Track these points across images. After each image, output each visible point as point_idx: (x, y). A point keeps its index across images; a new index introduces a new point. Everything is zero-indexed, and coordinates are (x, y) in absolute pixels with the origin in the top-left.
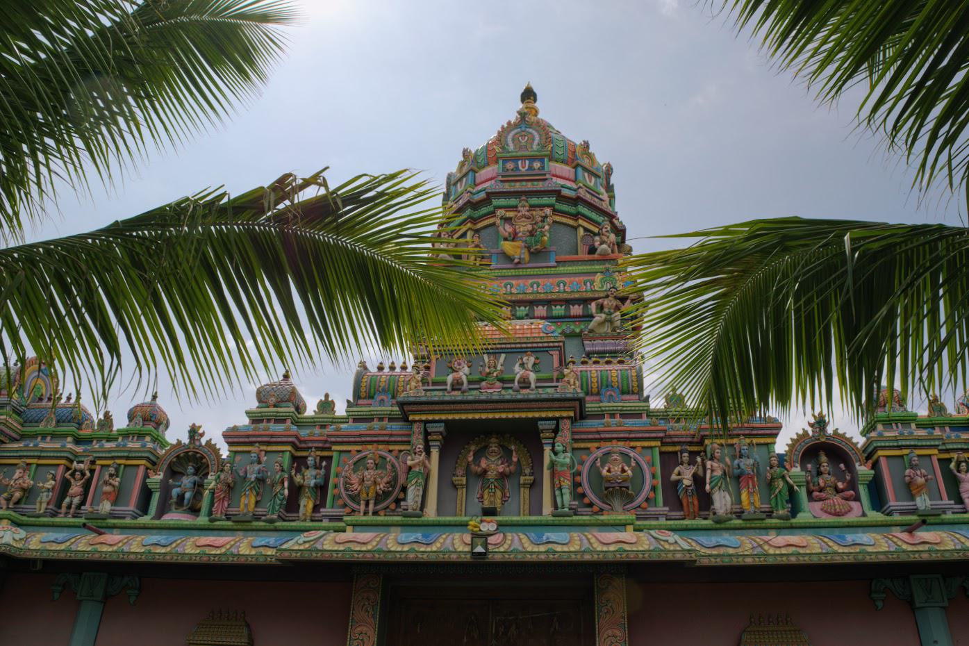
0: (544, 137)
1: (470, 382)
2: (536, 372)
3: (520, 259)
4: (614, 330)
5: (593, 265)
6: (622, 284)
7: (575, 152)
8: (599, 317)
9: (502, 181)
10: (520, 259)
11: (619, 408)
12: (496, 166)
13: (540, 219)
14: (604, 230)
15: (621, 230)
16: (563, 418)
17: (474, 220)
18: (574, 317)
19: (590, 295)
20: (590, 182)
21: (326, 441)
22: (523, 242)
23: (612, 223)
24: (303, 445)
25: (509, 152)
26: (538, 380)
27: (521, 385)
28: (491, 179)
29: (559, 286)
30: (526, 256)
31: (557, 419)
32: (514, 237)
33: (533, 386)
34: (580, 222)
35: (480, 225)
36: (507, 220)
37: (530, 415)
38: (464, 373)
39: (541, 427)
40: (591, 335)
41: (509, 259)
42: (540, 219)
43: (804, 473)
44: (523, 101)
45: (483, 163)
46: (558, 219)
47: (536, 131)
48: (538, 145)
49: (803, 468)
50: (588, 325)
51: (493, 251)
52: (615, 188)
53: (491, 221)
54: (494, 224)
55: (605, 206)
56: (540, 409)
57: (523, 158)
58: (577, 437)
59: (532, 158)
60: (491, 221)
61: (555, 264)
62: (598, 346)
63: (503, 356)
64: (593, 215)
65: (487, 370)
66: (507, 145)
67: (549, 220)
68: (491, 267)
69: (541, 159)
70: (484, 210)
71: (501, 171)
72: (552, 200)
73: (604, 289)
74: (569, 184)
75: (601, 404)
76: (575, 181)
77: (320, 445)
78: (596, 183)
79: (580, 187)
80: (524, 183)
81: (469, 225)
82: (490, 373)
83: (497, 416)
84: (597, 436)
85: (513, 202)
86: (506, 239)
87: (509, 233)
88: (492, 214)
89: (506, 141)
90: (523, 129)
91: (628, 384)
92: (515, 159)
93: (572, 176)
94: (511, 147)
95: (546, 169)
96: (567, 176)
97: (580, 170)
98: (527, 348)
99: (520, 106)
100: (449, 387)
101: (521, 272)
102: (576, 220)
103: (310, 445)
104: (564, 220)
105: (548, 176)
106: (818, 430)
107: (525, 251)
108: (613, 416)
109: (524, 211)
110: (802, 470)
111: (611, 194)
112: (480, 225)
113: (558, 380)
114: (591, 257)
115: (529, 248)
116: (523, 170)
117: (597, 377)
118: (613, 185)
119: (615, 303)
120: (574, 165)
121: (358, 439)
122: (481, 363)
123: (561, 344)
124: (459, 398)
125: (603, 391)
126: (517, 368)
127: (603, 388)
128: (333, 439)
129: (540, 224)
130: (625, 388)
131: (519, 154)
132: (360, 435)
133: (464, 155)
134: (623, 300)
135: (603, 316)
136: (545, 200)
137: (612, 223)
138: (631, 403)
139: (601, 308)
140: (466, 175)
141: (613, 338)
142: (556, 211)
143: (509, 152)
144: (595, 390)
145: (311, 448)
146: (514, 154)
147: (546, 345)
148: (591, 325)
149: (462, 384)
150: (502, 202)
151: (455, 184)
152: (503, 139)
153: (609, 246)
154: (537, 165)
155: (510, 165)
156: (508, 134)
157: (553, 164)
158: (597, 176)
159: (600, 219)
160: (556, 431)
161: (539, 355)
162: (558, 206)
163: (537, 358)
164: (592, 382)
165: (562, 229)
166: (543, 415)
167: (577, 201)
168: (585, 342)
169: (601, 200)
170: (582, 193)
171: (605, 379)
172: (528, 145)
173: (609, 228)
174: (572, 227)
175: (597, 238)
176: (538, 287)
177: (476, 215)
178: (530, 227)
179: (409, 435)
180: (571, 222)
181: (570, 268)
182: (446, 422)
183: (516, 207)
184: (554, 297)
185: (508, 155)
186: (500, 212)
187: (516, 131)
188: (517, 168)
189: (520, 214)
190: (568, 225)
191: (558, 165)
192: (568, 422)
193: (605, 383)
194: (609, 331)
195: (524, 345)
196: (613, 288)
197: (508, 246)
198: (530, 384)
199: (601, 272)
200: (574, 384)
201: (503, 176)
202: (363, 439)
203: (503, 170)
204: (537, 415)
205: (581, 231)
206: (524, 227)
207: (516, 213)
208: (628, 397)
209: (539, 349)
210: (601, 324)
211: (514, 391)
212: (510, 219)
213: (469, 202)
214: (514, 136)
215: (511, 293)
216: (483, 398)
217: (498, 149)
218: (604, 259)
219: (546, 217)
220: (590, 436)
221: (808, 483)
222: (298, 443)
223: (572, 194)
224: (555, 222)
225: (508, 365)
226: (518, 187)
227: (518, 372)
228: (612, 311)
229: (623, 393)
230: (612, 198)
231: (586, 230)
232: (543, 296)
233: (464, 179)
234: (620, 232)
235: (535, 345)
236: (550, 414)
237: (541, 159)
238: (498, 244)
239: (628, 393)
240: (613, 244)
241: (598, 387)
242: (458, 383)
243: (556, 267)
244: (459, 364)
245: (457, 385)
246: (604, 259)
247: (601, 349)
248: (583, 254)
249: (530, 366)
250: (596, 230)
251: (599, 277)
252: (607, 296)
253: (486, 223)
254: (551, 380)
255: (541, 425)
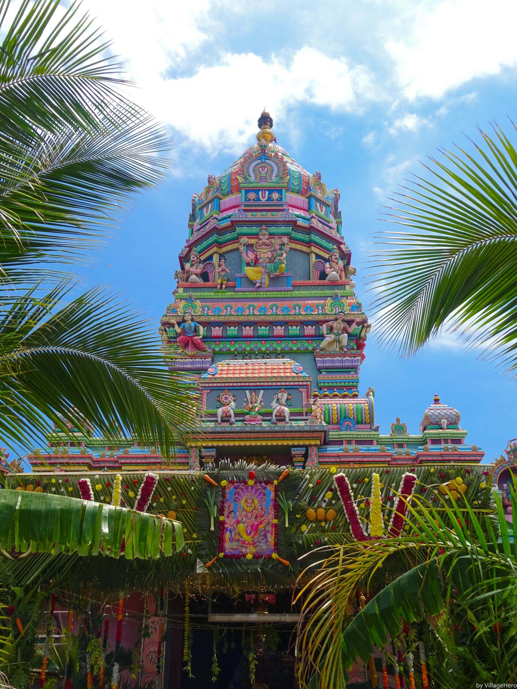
0: (281, 169)
1: (236, 415)
2: (288, 406)
3: (261, 283)
4: (341, 348)
5: (324, 290)
6: (349, 308)
7: (308, 183)
8: (329, 338)
9: (244, 210)
10: (261, 283)
11: (355, 436)
12: (239, 195)
13: (278, 247)
14: (333, 257)
15: (347, 254)
16: (311, 446)
17: (220, 245)
18: (307, 336)
19: (321, 318)
20: (322, 211)
21: (116, 462)
22: (263, 267)
23: (340, 249)
24: (97, 465)
25: (251, 183)
26: (292, 414)
27: (278, 418)
28: (235, 207)
29: (295, 309)
30: (266, 281)
31: (307, 447)
32: (256, 262)
33: (287, 419)
34: (313, 248)
35: (224, 249)
36: (249, 246)
37: (285, 443)
38: (231, 408)
39: (293, 453)
40: (322, 352)
41: (252, 283)
42: (278, 247)
43: (500, 492)
44: (260, 126)
45: (226, 191)
46: (293, 246)
47: (275, 163)
48: (277, 176)
49: (501, 488)
50: (320, 343)
51: (237, 275)
52: (342, 215)
53: (235, 246)
54: (238, 249)
55: (333, 234)
56: (293, 438)
57: (264, 189)
58: (321, 460)
59: (271, 190)
60: (235, 246)
61: (291, 288)
62: (328, 361)
63: (262, 392)
64: (324, 243)
65: (250, 406)
66: (249, 175)
67: (286, 248)
68: (236, 289)
69: (279, 191)
70: (229, 236)
71: (243, 200)
72: (289, 229)
73: (334, 312)
74: (301, 213)
75: (341, 433)
76: (308, 211)
77: (111, 465)
78: (326, 214)
79: (313, 217)
80: (264, 213)
81: (215, 249)
82: (252, 408)
83: (259, 443)
84: (338, 460)
85: (254, 230)
86: (248, 265)
87: (252, 260)
88: (236, 240)
89: (248, 172)
90: (263, 160)
91: (362, 418)
92: (256, 190)
93: (306, 207)
94: (252, 178)
95: (284, 200)
96: (301, 206)
97: (313, 200)
98: (281, 386)
99: (257, 130)
100: (219, 419)
101: (262, 295)
102: (309, 247)
103: (102, 465)
104: (299, 247)
105: (285, 207)
106: (513, 457)
107: (266, 276)
108: (349, 442)
109: (264, 239)
110: (499, 489)
111: (339, 220)
112: (224, 249)
113: (307, 414)
114: (322, 282)
115: (269, 274)
116: (263, 200)
117: (337, 409)
118: (340, 212)
119: (343, 325)
120: (307, 195)
121: (144, 461)
122: (245, 399)
123: (309, 383)
124: (229, 429)
125: (342, 422)
126: (274, 404)
127: (342, 419)
128: (123, 461)
129: (279, 252)
130: (360, 419)
131: (260, 185)
132: (145, 458)
133: (209, 181)
134: (350, 323)
135: (333, 336)
136: (283, 229)
137: (340, 249)
138: (364, 433)
139: (331, 329)
140: (211, 201)
141: (340, 355)
142: (292, 240)
143: (251, 183)
144: (335, 420)
145: (104, 467)
146: (255, 185)
147: (296, 383)
148: (323, 344)
149: (230, 416)
150: (245, 230)
151: (201, 209)
152: (245, 169)
153: (337, 273)
154: (275, 196)
155: (252, 195)
156: (250, 165)
157: (289, 194)
158: (327, 205)
159: (330, 246)
160: (306, 456)
161: (290, 391)
162: (294, 235)
163: (289, 395)
164: (332, 414)
165: (298, 255)
166: (296, 443)
167: (311, 230)
168: (317, 359)
169: (330, 228)
170: (315, 223)
171: (343, 411)
172: (268, 176)
173: (337, 256)
174: (305, 253)
175: (327, 265)
176: (276, 309)
177: (222, 240)
178: (270, 255)
179: (187, 457)
180: (305, 249)
181: (304, 292)
182: (217, 448)
183: (257, 235)
184: (291, 318)
185: (250, 185)
186: (244, 240)
187: (257, 162)
188: (258, 199)
189: (261, 242)
190: (302, 252)
191: (294, 195)
192: (315, 449)
193: (343, 415)
194: (338, 349)
195: (279, 384)
196: (341, 312)
197: (250, 272)
198: (285, 417)
199: (331, 297)
200: (320, 418)
201: (245, 205)
202: (148, 461)
203: (246, 200)
204: (290, 443)
205: (313, 257)
206: (264, 254)
207: (257, 240)
208: (361, 426)
209: (291, 387)
210: (330, 344)
211: (272, 423)
212: (252, 245)
213: (215, 228)
214: (255, 166)
215: (254, 315)
216: (248, 429)
217: (240, 179)
218: (334, 284)
219: (284, 244)
220: (332, 460)
221: (503, 499)
222: (92, 463)
223: (306, 224)
224: (291, 249)
225: (267, 401)
226: (258, 216)
227: (276, 407)
228: (340, 332)
229: (357, 423)
230: (339, 223)
231: (318, 256)
232: (281, 318)
233: (210, 205)
234: (346, 257)
235: (288, 384)
236: (301, 443)
237: (279, 191)
238: (241, 268)
239: (362, 423)
240: (341, 271)
241: (337, 418)
242: (226, 416)
243: (292, 291)
244: (226, 398)
245: (226, 419)
246: (334, 284)
247: (330, 365)
248: (315, 275)
249: (284, 401)
250: (327, 256)
251: (329, 301)
252: (336, 320)
253: (230, 247)
254: (301, 414)
255: (294, 451)
